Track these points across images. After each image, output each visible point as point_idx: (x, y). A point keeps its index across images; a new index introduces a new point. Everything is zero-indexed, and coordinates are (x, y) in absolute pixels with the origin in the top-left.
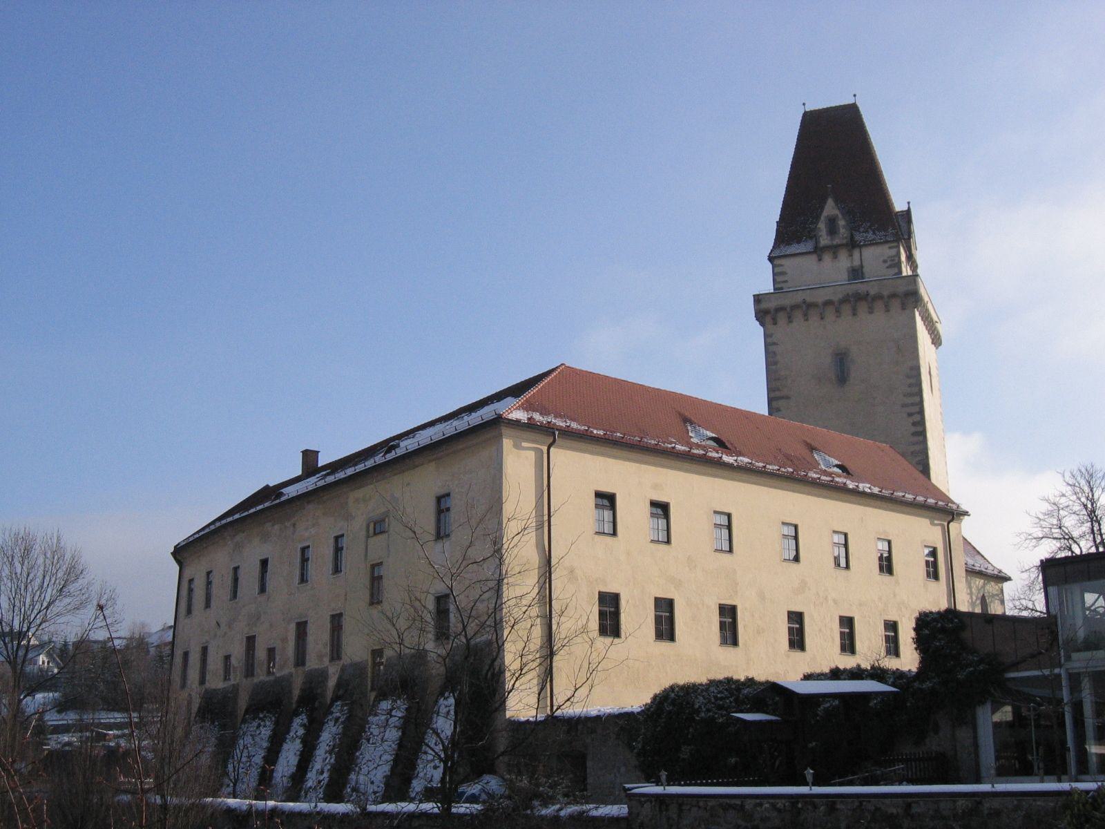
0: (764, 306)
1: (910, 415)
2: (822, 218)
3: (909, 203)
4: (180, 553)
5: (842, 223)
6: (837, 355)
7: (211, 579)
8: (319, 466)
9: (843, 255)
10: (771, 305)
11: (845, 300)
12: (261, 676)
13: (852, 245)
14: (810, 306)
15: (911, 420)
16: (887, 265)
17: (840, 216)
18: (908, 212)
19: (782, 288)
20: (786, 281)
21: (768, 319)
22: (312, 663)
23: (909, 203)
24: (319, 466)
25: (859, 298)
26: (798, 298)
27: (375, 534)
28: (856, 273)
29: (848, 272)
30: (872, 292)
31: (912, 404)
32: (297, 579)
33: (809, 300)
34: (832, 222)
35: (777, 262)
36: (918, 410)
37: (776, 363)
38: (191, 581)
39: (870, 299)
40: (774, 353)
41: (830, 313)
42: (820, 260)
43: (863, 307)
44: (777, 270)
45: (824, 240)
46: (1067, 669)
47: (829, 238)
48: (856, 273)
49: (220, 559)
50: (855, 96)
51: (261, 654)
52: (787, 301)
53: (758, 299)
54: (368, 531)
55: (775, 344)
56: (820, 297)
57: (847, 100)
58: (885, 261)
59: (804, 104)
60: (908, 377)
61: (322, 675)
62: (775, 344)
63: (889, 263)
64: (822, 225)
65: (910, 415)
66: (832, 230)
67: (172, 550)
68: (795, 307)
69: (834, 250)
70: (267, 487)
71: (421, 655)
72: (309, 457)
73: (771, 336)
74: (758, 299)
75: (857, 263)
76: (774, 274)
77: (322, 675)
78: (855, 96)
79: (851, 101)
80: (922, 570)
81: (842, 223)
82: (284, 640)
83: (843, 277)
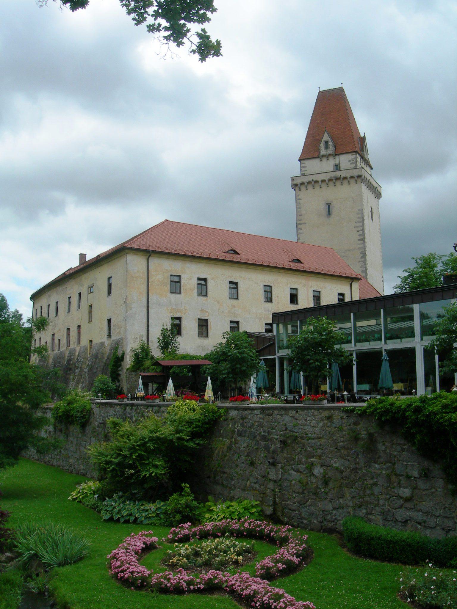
0: (295, 182)
1: (358, 231)
2: (322, 142)
3: (364, 133)
4: (35, 297)
5: (330, 144)
6: (327, 204)
7: (71, 301)
8: (87, 260)
9: (331, 159)
10: (298, 181)
11: (330, 180)
12: (56, 351)
13: (336, 154)
14: (316, 182)
15: (358, 233)
16: (350, 163)
17: (330, 140)
18: (364, 137)
19: (304, 174)
20: (306, 171)
21: (297, 188)
22: (72, 346)
23: (364, 133)
24: (87, 260)
25: (338, 179)
26: (310, 179)
27: (91, 293)
28: (337, 167)
29: (333, 166)
30: (342, 176)
31: (359, 227)
32: (67, 311)
33: (315, 179)
34: (327, 142)
35: (302, 162)
36: (361, 229)
37: (300, 208)
38: (37, 310)
39: (341, 179)
40: (300, 203)
41: (324, 185)
42: (321, 161)
43: (338, 183)
44: (302, 165)
45: (323, 152)
46: (278, 356)
47: (325, 151)
48: (337, 167)
49: (53, 297)
50: (342, 84)
51: (56, 341)
52: (305, 180)
53: (293, 179)
54: (88, 292)
55: (300, 199)
56: (319, 178)
57: (338, 86)
58: (349, 161)
59: (319, 88)
60: (358, 214)
61: (74, 350)
62: (300, 199)
63: (352, 162)
64: (322, 145)
65: (358, 231)
66: (327, 147)
67: (30, 296)
68: (309, 183)
69: (327, 156)
70: (71, 268)
71: (102, 344)
72: (82, 256)
73: (299, 195)
74: (293, 179)
75: (337, 162)
76: (301, 167)
77: (74, 350)
78: (342, 84)
79: (340, 86)
80: (211, 324)
81: (330, 144)
82: (63, 336)
83: (331, 168)
